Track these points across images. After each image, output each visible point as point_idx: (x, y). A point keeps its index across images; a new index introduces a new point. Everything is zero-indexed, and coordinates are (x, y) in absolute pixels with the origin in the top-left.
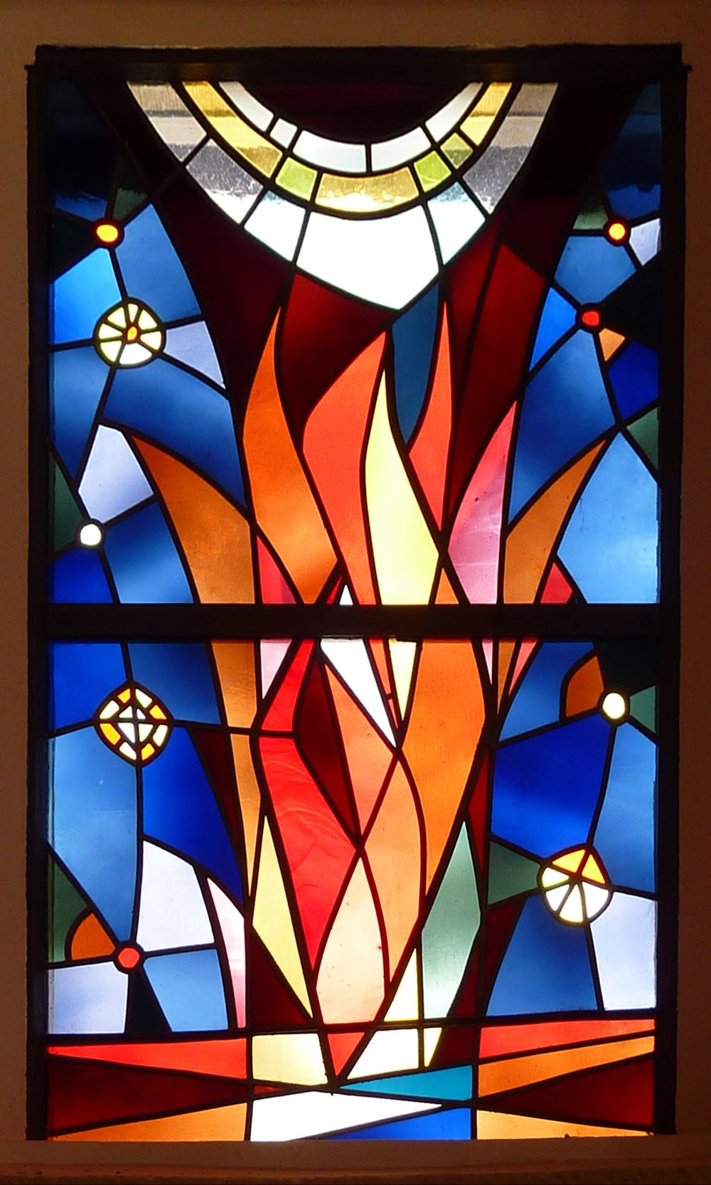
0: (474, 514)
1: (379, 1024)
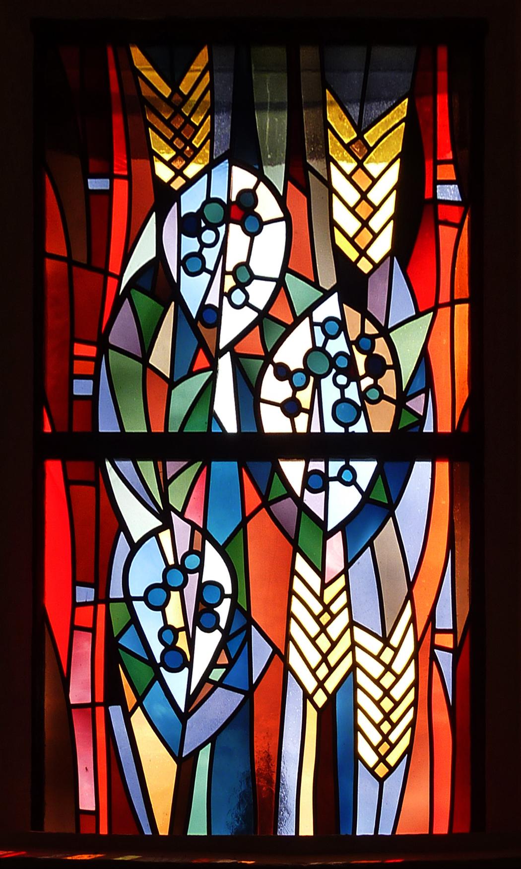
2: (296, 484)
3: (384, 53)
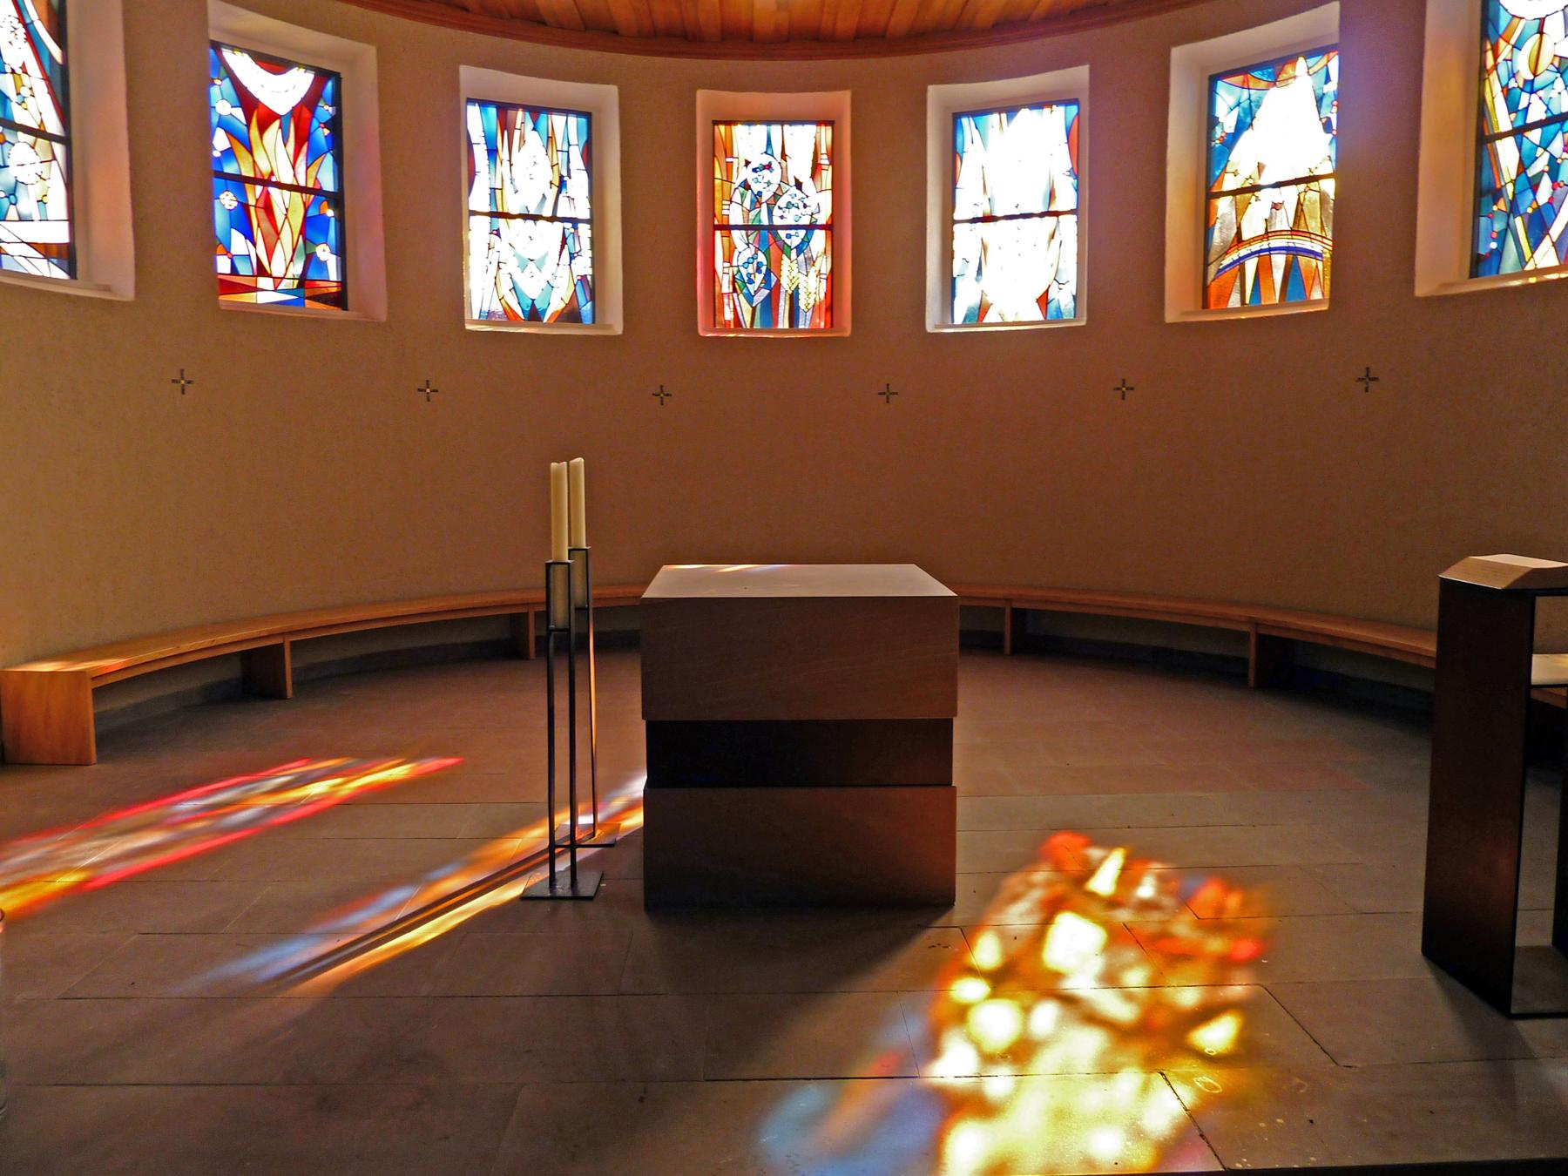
0: (300, 165)
1: (284, 278)
2: (784, 237)
3: (1332, 54)
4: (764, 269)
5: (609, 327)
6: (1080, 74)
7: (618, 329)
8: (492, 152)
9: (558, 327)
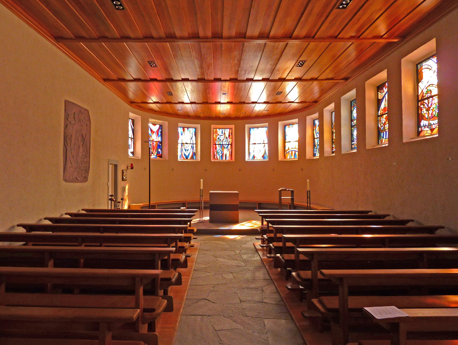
4: (221, 151)
5: (198, 160)
6: (267, 124)
7: (199, 160)
8: (182, 134)
9: (190, 160)
